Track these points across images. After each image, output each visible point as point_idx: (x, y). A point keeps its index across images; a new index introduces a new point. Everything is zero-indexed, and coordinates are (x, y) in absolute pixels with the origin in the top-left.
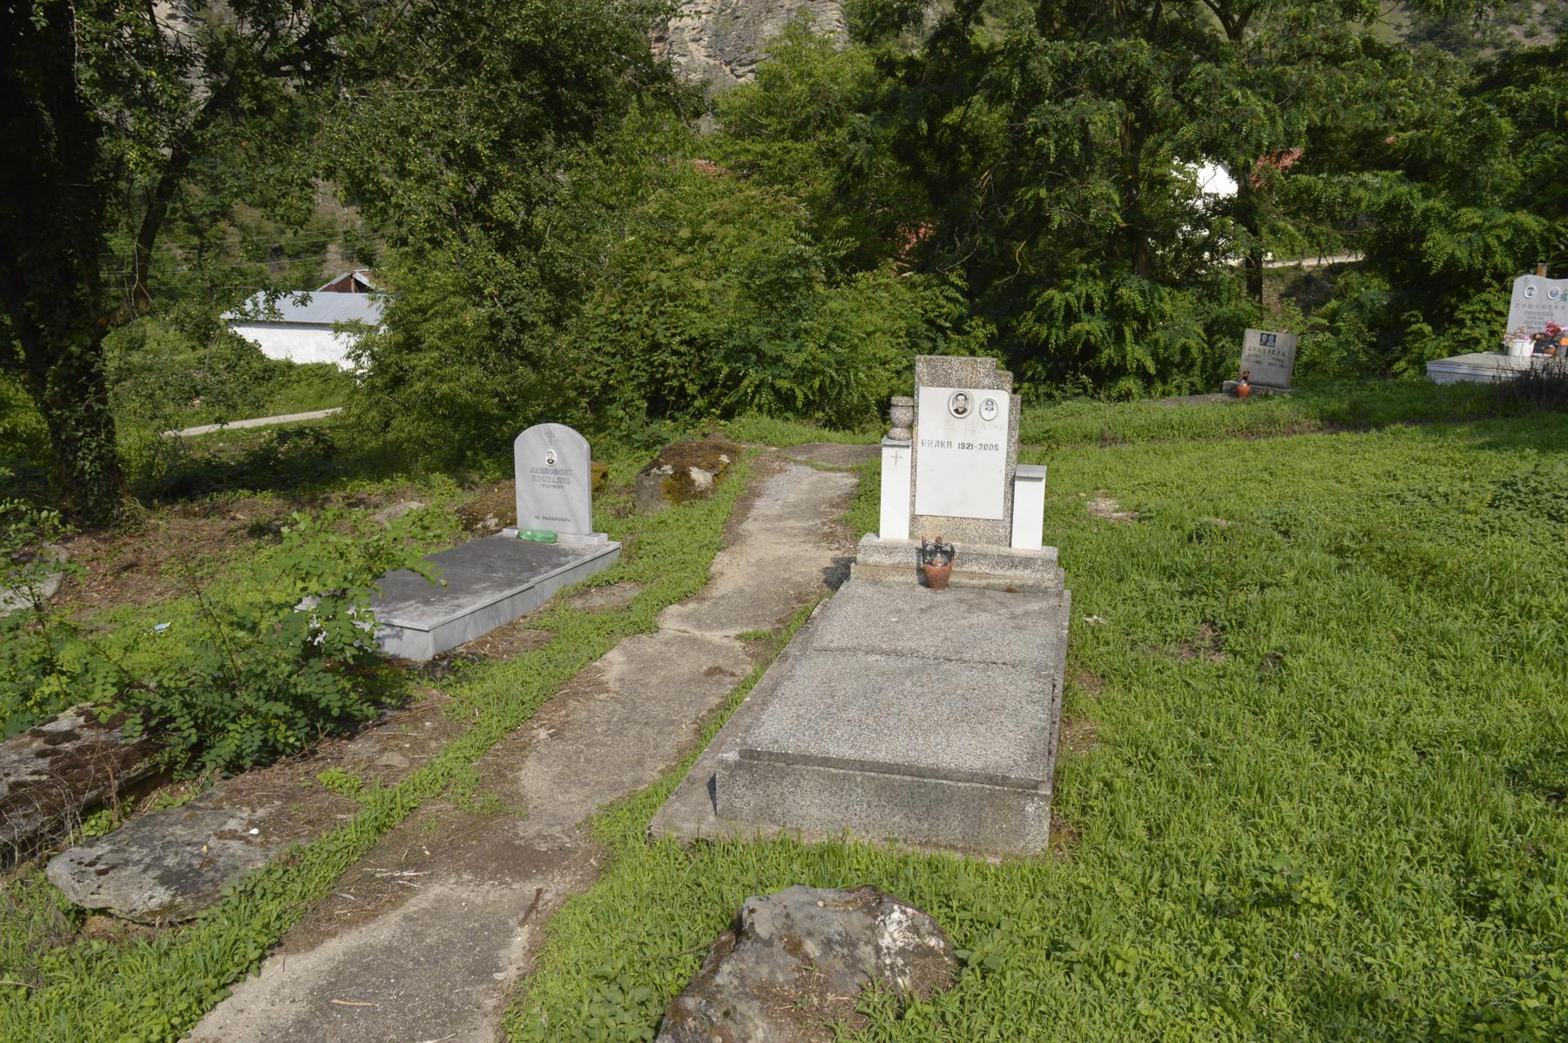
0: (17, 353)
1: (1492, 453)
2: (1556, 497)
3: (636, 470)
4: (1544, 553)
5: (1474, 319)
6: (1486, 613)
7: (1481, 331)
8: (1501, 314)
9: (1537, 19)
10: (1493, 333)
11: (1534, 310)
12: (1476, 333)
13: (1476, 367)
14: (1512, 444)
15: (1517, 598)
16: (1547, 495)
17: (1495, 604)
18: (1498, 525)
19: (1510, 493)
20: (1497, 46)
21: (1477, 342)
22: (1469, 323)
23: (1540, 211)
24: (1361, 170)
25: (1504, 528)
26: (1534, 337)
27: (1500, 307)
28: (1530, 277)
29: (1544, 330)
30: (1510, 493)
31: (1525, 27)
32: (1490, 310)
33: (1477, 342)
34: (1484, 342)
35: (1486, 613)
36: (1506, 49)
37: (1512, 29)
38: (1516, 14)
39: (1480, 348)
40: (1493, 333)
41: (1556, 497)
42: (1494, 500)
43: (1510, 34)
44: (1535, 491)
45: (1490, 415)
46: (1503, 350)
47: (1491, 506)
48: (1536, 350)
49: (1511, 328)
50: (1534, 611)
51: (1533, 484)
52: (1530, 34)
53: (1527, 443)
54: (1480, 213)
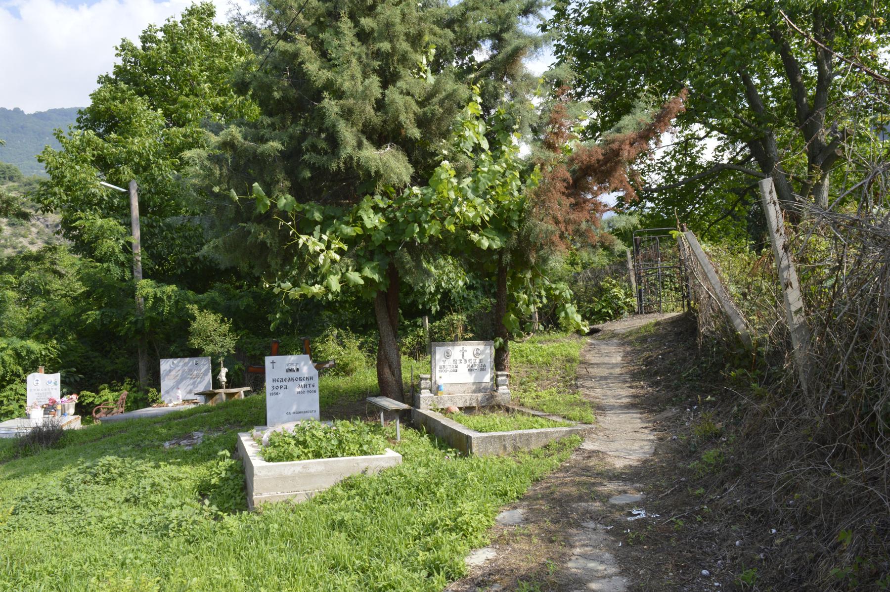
0: (227, 375)
1: (15, 481)
2: (51, 500)
3: (640, 425)
4: (45, 535)
5: (8, 400)
6: (9, 585)
7: (14, 406)
8: (23, 395)
9: (34, 236)
10: (21, 406)
11: (41, 392)
12: (11, 408)
13: (9, 429)
14: (27, 473)
15: (27, 570)
16: (45, 500)
17: (15, 577)
18: (17, 525)
19: (24, 504)
20: (14, 248)
21: (12, 413)
22: (5, 402)
23: (37, 338)
24: (189, 289)
25: (21, 527)
26: (42, 407)
27: (23, 392)
28: (36, 374)
29: (47, 402)
30: (24, 504)
31: (29, 239)
32: (17, 393)
33: (12, 413)
34: (16, 413)
35: (9, 585)
36: (20, 249)
37: (21, 239)
38: (23, 232)
39: (14, 416)
40: (21, 406)
41: (51, 500)
42: (15, 510)
43: (21, 242)
44: (38, 499)
45: (15, 457)
46: (28, 416)
47: (13, 514)
48: (45, 414)
49: (29, 403)
50: (37, 574)
51: (36, 495)
52: (32, 243)
53: (35, 471)
54: (5, 341)
